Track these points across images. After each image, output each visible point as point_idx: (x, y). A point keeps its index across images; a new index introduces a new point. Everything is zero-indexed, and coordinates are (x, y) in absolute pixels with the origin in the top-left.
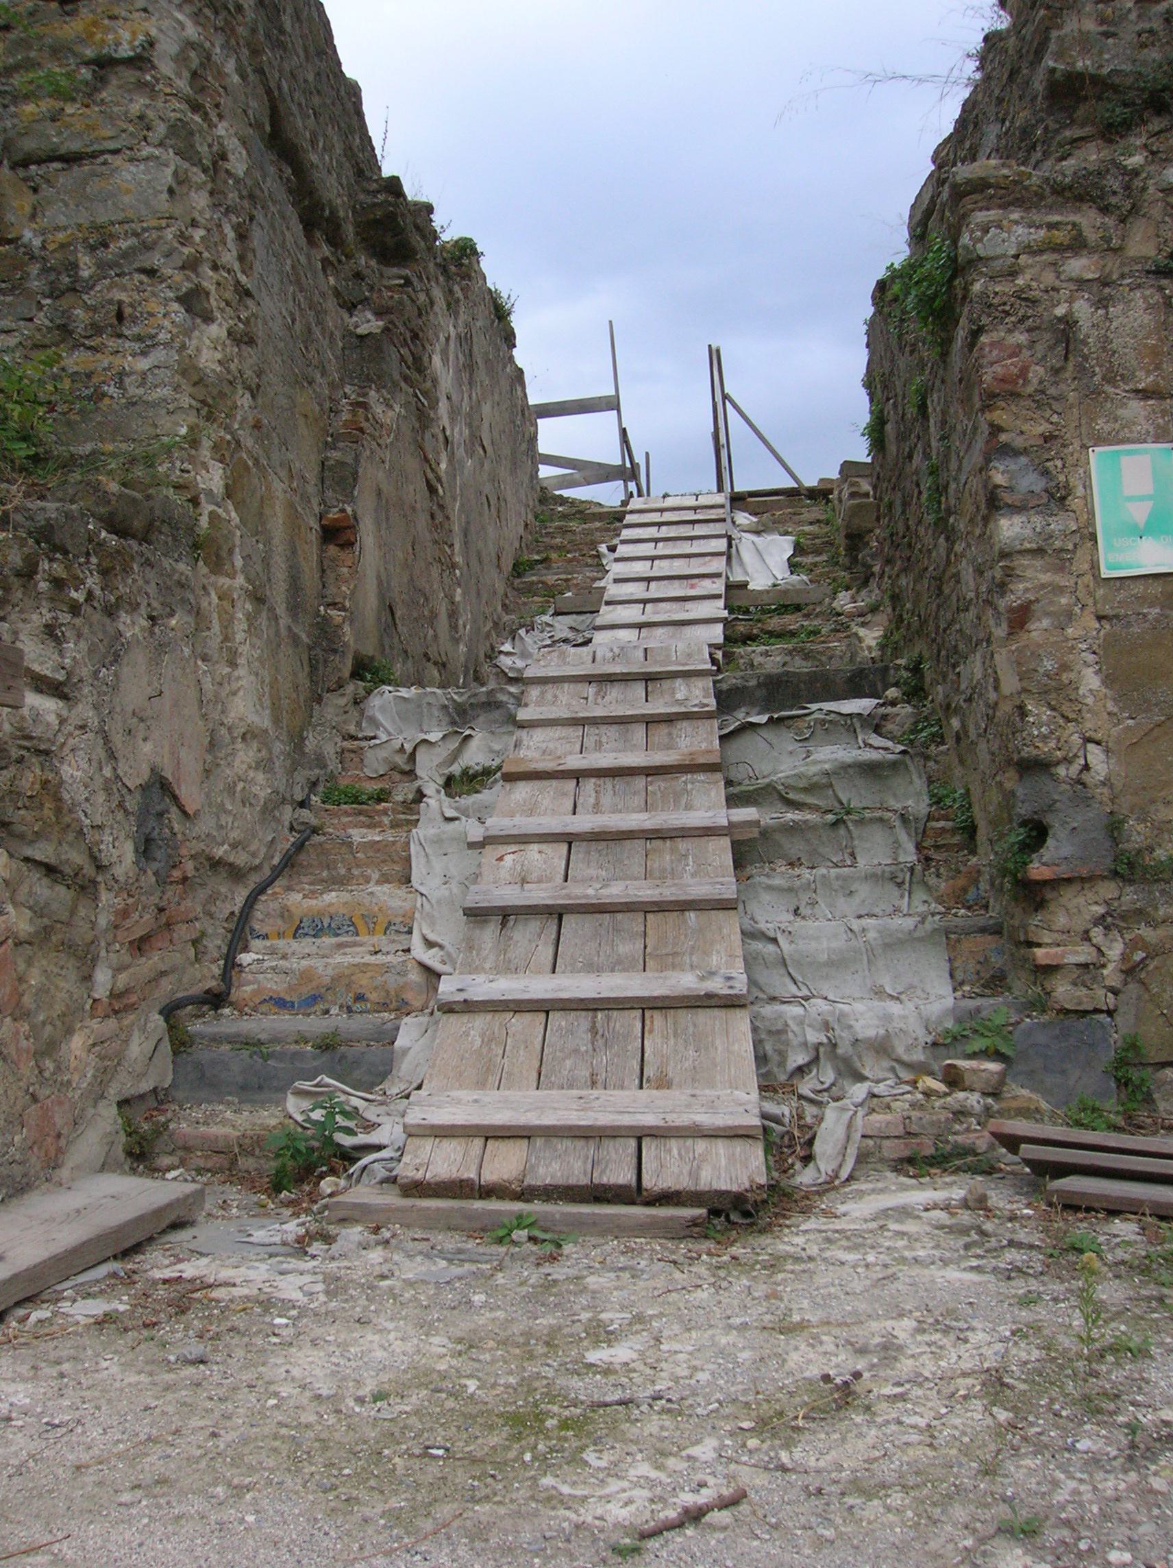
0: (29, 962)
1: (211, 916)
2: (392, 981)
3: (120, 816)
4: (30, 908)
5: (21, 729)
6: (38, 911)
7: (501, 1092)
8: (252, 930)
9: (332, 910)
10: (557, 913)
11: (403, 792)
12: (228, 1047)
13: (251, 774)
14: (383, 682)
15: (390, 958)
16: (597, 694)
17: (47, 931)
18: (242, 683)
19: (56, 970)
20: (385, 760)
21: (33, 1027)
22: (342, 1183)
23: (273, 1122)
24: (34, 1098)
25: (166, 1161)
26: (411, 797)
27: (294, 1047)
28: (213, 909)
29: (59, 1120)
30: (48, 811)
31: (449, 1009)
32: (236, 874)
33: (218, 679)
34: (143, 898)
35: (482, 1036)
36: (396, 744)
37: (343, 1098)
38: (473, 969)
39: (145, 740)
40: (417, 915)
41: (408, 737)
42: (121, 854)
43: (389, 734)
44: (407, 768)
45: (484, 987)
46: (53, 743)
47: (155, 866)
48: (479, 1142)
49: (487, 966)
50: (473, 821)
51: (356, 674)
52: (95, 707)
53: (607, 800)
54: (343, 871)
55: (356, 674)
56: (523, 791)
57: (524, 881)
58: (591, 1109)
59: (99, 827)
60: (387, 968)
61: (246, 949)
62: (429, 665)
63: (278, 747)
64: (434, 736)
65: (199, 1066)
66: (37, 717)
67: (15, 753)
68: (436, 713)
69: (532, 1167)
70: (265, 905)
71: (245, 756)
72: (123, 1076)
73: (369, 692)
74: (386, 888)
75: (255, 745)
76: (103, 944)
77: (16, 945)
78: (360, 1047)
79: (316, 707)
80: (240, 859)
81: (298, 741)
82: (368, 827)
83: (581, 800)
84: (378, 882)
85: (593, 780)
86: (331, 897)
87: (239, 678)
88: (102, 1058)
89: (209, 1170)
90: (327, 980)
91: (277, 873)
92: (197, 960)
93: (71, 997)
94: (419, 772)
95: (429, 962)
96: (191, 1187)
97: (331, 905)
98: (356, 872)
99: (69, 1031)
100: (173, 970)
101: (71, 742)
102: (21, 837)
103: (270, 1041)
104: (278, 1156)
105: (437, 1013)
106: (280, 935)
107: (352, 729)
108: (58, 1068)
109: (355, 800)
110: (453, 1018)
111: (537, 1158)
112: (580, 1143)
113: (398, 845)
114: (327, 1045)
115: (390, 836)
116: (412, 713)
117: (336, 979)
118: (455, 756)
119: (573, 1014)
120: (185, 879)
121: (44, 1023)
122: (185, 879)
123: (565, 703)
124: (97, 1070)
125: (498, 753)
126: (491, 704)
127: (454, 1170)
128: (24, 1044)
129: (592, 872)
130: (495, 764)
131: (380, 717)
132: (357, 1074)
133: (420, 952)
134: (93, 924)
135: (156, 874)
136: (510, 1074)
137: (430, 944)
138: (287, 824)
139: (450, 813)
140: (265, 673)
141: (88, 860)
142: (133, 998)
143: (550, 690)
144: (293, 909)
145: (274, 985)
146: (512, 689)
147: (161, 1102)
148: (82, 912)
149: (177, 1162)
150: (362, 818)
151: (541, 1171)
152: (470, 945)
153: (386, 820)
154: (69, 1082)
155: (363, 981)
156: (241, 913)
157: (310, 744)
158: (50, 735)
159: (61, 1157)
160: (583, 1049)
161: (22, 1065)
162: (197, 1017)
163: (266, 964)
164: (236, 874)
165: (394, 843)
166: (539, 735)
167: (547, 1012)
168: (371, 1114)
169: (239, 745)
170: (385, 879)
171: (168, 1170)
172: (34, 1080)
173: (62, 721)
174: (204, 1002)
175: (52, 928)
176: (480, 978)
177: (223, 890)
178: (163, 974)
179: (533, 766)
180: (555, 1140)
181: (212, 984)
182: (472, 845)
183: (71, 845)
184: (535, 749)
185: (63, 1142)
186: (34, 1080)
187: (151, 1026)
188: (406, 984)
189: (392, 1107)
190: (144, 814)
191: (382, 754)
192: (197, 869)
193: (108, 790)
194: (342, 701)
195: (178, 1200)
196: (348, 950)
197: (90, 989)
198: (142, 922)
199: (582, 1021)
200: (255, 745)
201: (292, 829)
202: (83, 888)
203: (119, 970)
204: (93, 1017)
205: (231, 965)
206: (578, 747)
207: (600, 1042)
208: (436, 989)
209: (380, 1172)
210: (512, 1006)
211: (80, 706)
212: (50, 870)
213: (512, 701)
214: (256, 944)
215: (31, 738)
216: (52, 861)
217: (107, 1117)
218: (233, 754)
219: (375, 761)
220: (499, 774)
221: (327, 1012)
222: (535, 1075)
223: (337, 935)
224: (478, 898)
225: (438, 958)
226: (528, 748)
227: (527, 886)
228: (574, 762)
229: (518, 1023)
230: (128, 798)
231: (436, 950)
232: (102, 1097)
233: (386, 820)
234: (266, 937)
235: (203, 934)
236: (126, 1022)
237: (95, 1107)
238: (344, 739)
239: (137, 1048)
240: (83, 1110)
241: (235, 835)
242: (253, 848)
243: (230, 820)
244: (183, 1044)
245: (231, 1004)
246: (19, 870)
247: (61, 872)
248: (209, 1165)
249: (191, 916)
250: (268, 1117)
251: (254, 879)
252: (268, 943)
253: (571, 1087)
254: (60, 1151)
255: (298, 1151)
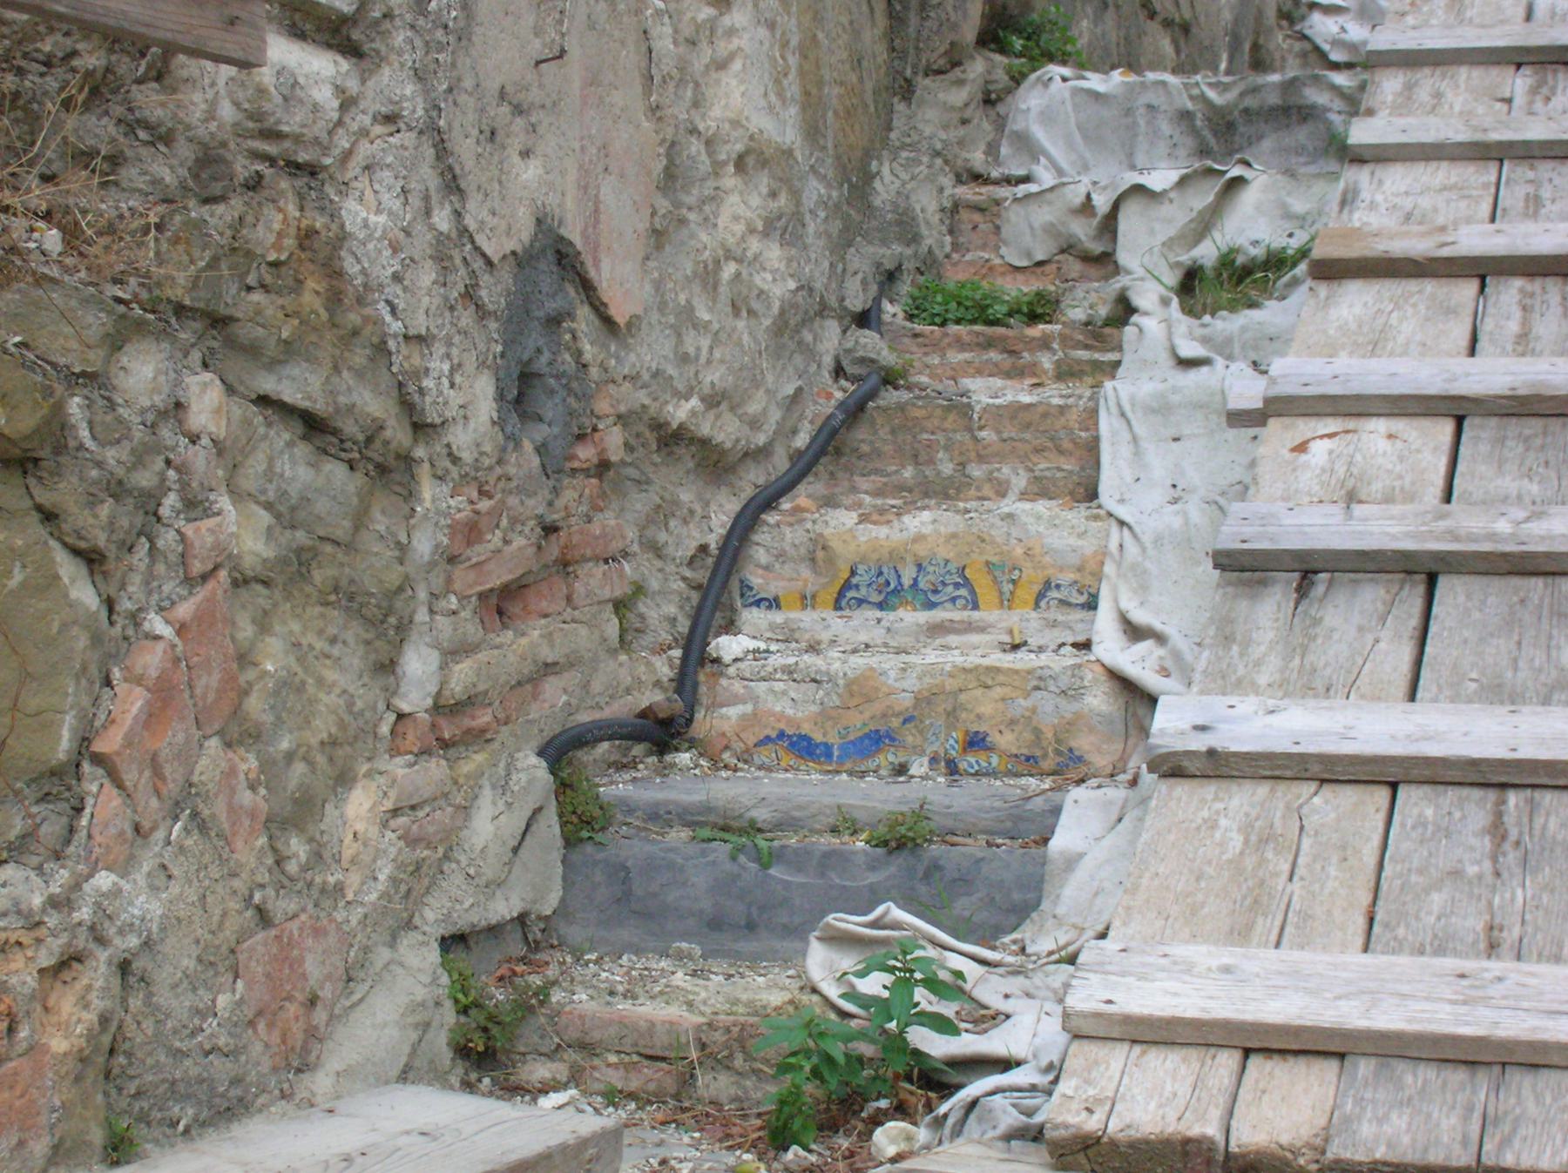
0: (263, 624)
1: (657, 550)
2: (1049, 709)
3: (467, 318)
4: (268, 506)
5: (257, 116)
6: (286, 514)
7: (1283, 953)
8: (745, 587)
9: (922, 550)
10: (1425, 572)
11: (1085, 302)
12: (685, 834)
13: (754, 245)
14: (1050, 57)
15: (1044, 659)
16: (1534, 91)
17: (299, 564)
18: (742, 42)
19: (320, 645)
20: (1050, 230)
21: (266, 764)
22: (922, 1134)
23: (776, 998)
24: (264, 916)
25: (540, 1071)
26: (1103, 311)
27: (827, 841)
28: (662, 537)
29: (314, 968)
30: (311, 297)
31: (1173, 768)
32: (716, 465)
33: (687, 31)
34: (513, 501)
35: (1246, 829)
36: (1076, 195)
37: (931, 952)
38: (1228, 683)
39: (526, 154)
40: (1109, 569)
41: (1101, 180)
42: (469, 403)
43: (1060, 172)
44: (1097, 248)
45: (1251, 725)
46: (326, 150)
47: (541, 432)
48: (1227, 1061)
49: (1263, 680)
50: (1241, 368)
51: (990, 38)
52: (419, 75)
53: (1548, 326)
54: (947, 468)
55: (990, 38)
56: (1355, 301)
57: (1352, 498)
58: (1486, 1001)
59: (420, 339)
60: (1038, 681)
61: (730, 627)
62: (1153, 27)
63: (814, 191)
64: (1161, 178)
65: (620, 872)
66: (292, 90)
67: (242, 168)
68: (1166, 128)
69: (1347, 1120)
70: (777, 535)
71: (740, 205)
72: (454, 882)
73: (1017, 79)
74: (1041, 506)
75: (764, 182)
76: (422, 595)
77: (236, 584)
78: (975, 847)
79: (900, 107)
80: (725, 430)
81: (857, 182)
82: (1008, 375)
83: (1487, 326)
84: (1024, 496)
85: (1518, 283)
86: (921, 522)
87: (731, 32)
88: (411, 841)
89: (631, 1096)
90: (906, 701)
91: (804, 467)
92: (624, 643)
93: (350, 705)
94: (1123, 257)
95: (1133, 671)
96: (590, 1123)
97: (919, 538)
98: (976, 471)
99: (344, 779)
100: (572, 663)
101: (365, 149)
102: (252, 351)
103: (779, 826)
104: (784, 1068)
105: (1148, 778)
106: (807, 601)
107: (977, 158)
108: (317, 856)
109: (980, 313)
110: (1181, 789)
111: (1359, 1101)
112: (1459, 1075)
113: (1073, 417)
114: (899, 838)
115: (1054, 394)
116: (1114, 129)
117: (925, 700)
118: (1204, 225)
119: (1452, 793)
120: (603, 466)
121: (290, 757)
122: (603, 466)
123: (1459, 108)
124: (401, 866)
125: (1302, 220)
126: (1291, 112)
127: (1172, 1116)
128: (246, 797)
129: (1509, 484)
130: (1295, 243)
131: (1040, 134)
132: (963, 906)
133: (1111, 648)
134: (403, 550)
135: (541, 449)
136: (1306, 916)
137: (1134, 632)
138: (828, 361)
139: (1189, 350)
140: (790, 24)
141: (394, 409)
142: (484, 718)
143: (1427, 81)
144: (835, 544)
145: (790, 706)
146: (1340, 79)
147: (535, 947)
148: (380, 523)
149: (563, 1076)
150: (994, 355)
151: (1366, 1130)
152: (1226, 634)
153: (1047, 362)
154: (339, 888)
155: (985, 707)
156: (723, 549)
157: (886, 187)
158: (319, 130)
159: (316, 1048)
160: (1472, 870)
161: (239, 844)
162: (621, 767)
163: (775, 661)
164: (716, 465)
165: (1062, 409)
166: (1397, 181)
167: (1394, 786)
168: (989, 990)
169: (730, 180)
170: (1041, 489)
171: (544, 1090)
172: (263, 877)
173: (348, 103)
174: (636, 737)
175: (315, 552)
176: (1247, 705)
177: (686, 496)
178: (550, 668)
179: (1381, 247)
180: (1400, 1066)
181: (650, 697)
182: (1239, 418)
183: (359, 374)
184: (1387, 208)
185: (320, 1016)
186: (263, 877)
187: (519, 779)
188: (1078, 716)
189: (1038, 979)
190: (518, 317)
191: (1043, 215)
192: (629, 448)
193: (441, 258)
194: (958, 97)
195: (564, 1148)
196: (953, 639)
197: (391, 692)
198: (509, 553)
199: (1474, 809)
200: (764, 182)
201: (839, 372)
202: (382, 469)
203: (453, 653)
204: (395, 752)
205: (696, 659)
206: (1485, 208)
207: (1511, 857)
208: (1145, 732)
209: (1007, 1115)
210: (1315, 769)
211: (386, 71)
212: (313, 425)
213: (1338, 104)
214: (753, 617)
215: (273, 135)
216: (320, 406)
217: (416, 970)
218: (716, 198)
219: (1027, 231)
220: (1302, 268)
221: (901, 770)
222: (1361, 921)
223: (931, 605)
224: (1248, 531)
225: (1152, 662)
226: (1373, 206)
227: (1358, 510)
228: (1476, 240)
229: (1327, 807)
230: (485, 279)
231: (1147, 645)
232: (409, 925)
233: (1047, 362)
234: (774, 603)
235: (639, 590)
236: (466, 767)
237: (392, 943)
238: (959, 180)
239: (488, 826)
240: (366, 950)
241: (714, 377)
242: (753, 408)
243: (705, 343)
244: (588, 823)
245: (692, 744)
246: (247, 422)
247: (335, 432)
248: (634, 1084)
249: (616, 546)
250: (767, 989)
251: (753, 478)
252: (778, 617)
253: (1440, 951)
254: (312, 1034)
255: (829, 1060)
